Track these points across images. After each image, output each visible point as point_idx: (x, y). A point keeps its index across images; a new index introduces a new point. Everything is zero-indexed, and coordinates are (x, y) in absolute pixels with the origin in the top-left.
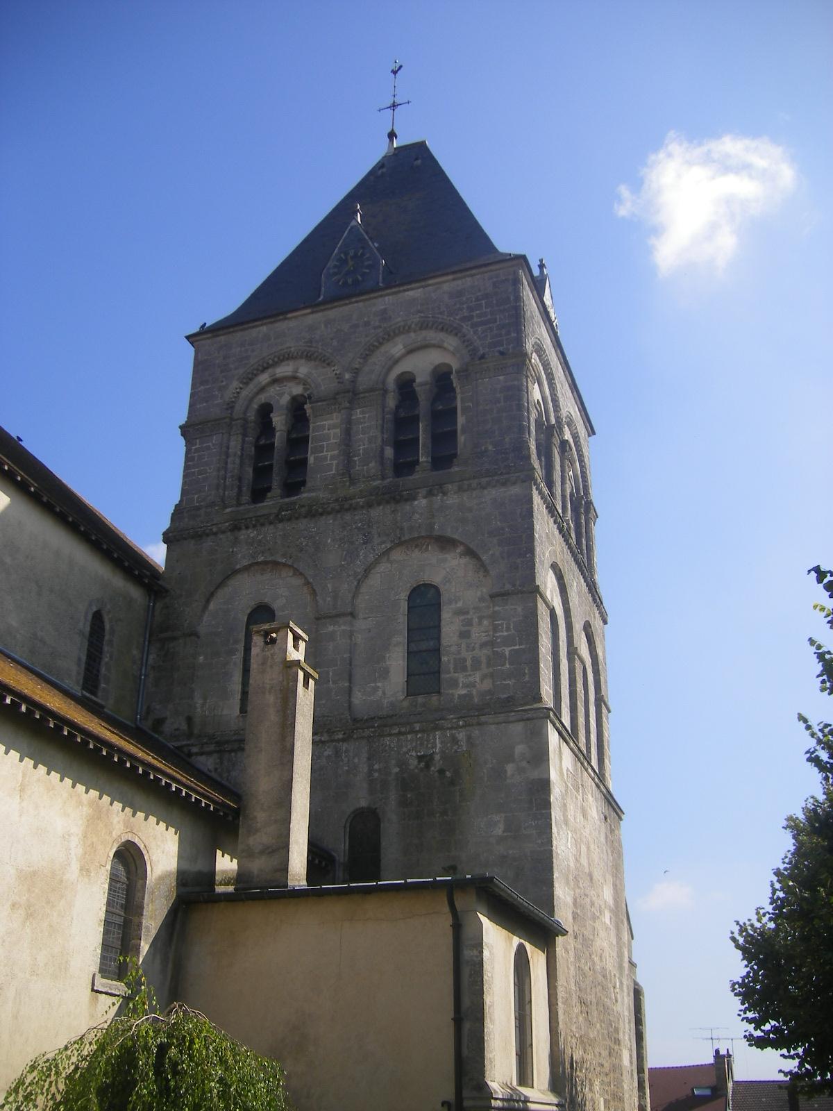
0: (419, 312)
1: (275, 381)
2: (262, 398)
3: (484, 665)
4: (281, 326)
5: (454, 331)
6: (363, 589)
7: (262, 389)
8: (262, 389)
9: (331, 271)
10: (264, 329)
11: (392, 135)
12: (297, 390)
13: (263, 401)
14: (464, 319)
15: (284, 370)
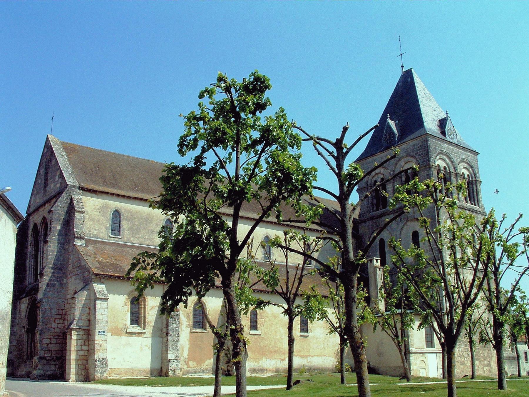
0: (406, 152)
1: (376, 174)
2: (374, 179)
3: (429, 251)
4: (374, 158)
5: (415, 157)
6: (402, 233)
7: (374, 176)
8: (374, 176)
9: (384, 139)
10: (371, 159)
11: (402, 67)
12: (382, 176)
13: (375, 180)
14: (416, 154)
15: (377, 171)
